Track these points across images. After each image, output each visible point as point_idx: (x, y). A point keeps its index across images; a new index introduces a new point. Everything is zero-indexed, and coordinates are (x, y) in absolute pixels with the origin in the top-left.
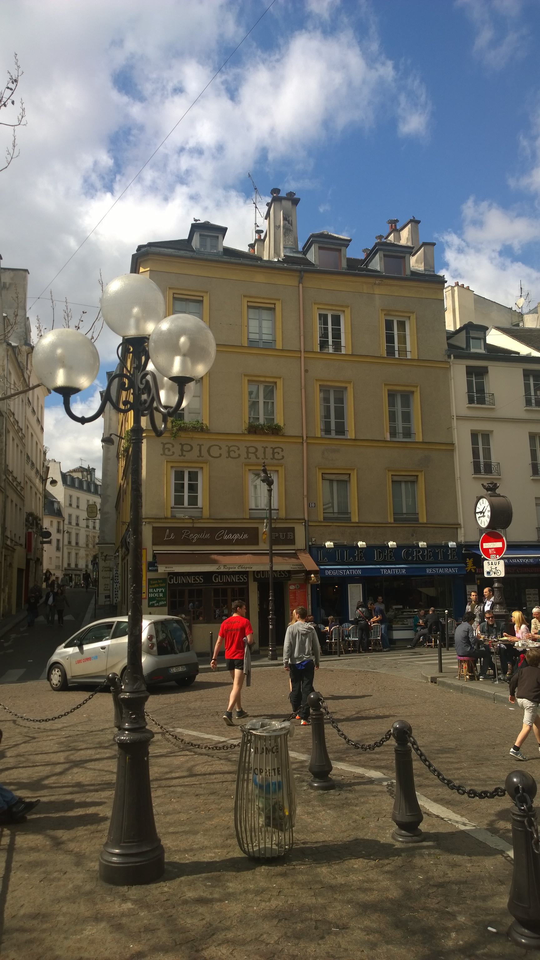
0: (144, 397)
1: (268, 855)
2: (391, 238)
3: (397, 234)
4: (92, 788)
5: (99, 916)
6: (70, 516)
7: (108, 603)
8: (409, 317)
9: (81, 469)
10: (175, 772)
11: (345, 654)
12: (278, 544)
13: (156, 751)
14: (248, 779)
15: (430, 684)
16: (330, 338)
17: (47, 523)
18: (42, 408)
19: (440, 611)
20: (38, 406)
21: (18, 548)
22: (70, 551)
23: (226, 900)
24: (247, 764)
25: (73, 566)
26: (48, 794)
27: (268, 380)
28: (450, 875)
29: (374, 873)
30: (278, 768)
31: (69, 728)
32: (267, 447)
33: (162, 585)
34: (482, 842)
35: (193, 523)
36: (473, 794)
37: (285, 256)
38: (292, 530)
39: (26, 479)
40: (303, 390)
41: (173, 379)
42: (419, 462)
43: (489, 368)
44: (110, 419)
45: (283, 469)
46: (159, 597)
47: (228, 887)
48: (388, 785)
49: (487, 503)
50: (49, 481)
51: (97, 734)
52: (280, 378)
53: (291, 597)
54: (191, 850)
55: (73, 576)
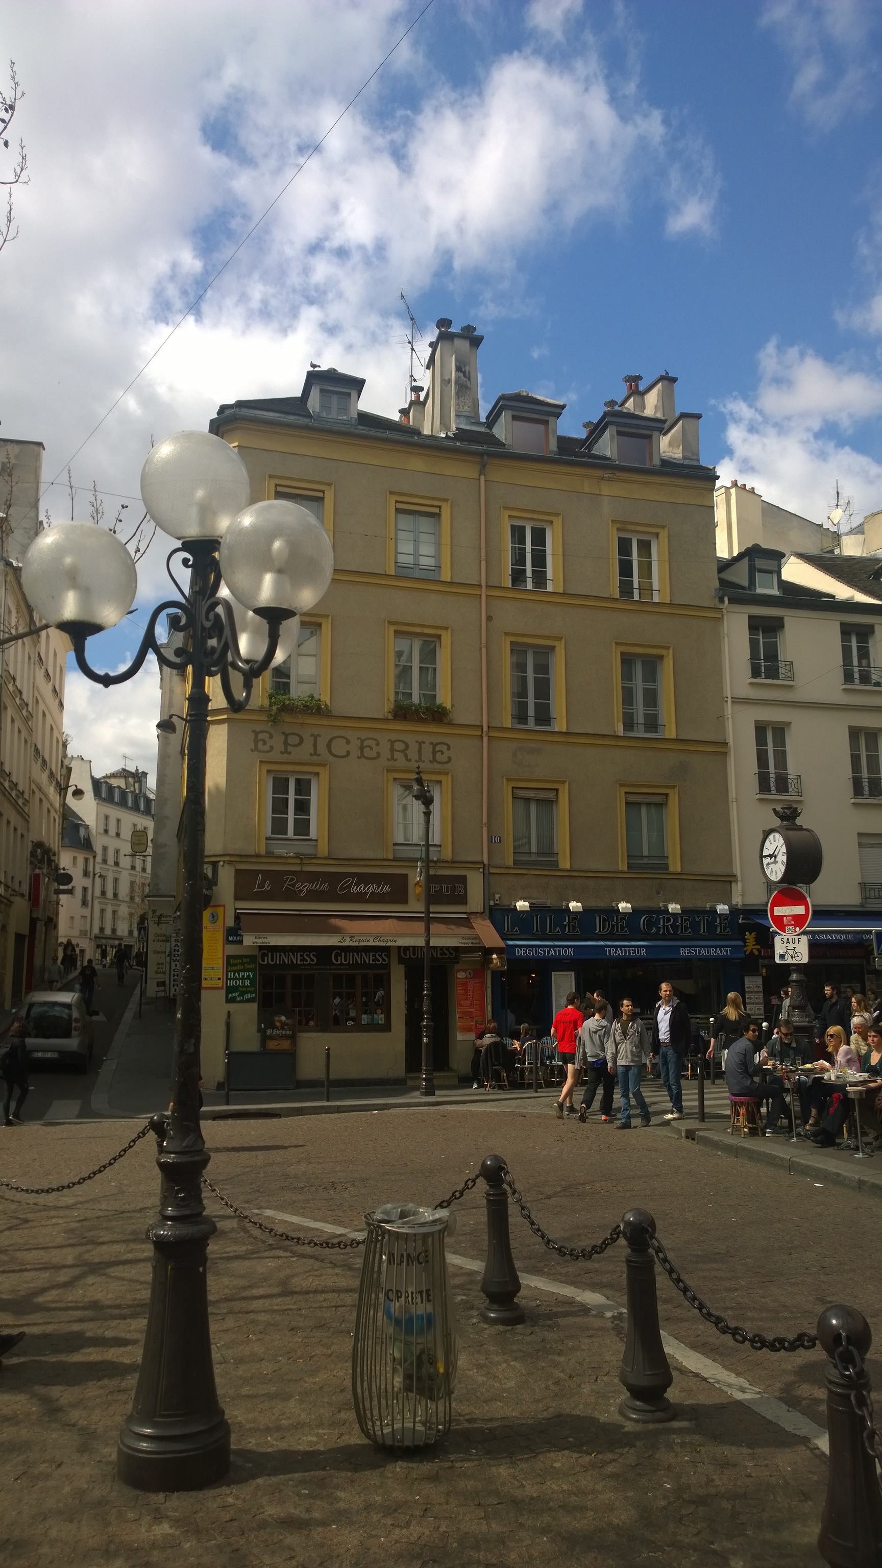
0: (213, 642)
1: (408, 1443)
2: (630, 405)
3: (638, 398)
4: (117, 1312)
5: (112, 1547)
6: (105, 849)
7: (162, 994)
8: (657, 535)
9: (124, 774)
10: (258, 1287)
11: (547, 1087)
12: (435, 903)
13: (228, 1249)
14: (377, 1304)
15: (684, 1140)
16: (528, 567)
17: (66, 860)
18: (61, 670)
19: (702, 1019)
20: (55, 666)
21: (17, 900)
22: (103, 907)
23: (334, 1522)
24: (375, 1276)
25: (108, 931)
26: (41, 1321)
27: (427, 631)
28: (718, 1483)
29: (589, 1478)
30: (428, 1291)
31: (86, 1206)
32: (424, 743)
33: (249, 966)
34: (771, 1422)
35: (302, 864)
36: (759, 1342)
37: (457, 429)
38: (463, 880)
39: (33, 787)
40: (484, 650)
41: (259, 611)
42: (669, 771)
43: (786, 619)
44: (171, 691)
45: (450, 779)
46: (244, 986)
47: (338, 1499)
48: (613, 1316)
49: (782, 841)
50: (71, 790)
51: (131, 1217)
52: (446, 628)
53: (460, 990)
54: (278, 1428)
55: (108, 949)
